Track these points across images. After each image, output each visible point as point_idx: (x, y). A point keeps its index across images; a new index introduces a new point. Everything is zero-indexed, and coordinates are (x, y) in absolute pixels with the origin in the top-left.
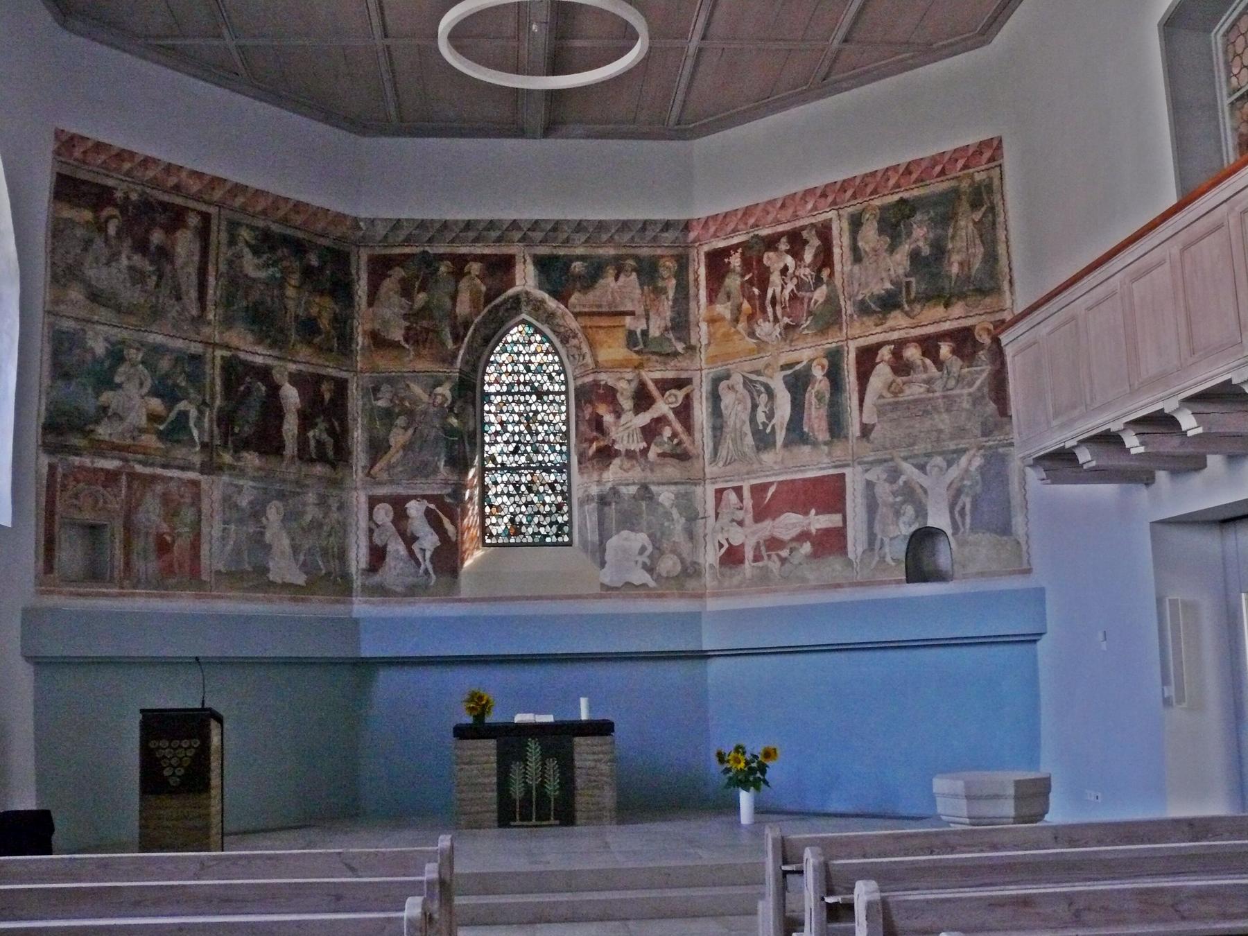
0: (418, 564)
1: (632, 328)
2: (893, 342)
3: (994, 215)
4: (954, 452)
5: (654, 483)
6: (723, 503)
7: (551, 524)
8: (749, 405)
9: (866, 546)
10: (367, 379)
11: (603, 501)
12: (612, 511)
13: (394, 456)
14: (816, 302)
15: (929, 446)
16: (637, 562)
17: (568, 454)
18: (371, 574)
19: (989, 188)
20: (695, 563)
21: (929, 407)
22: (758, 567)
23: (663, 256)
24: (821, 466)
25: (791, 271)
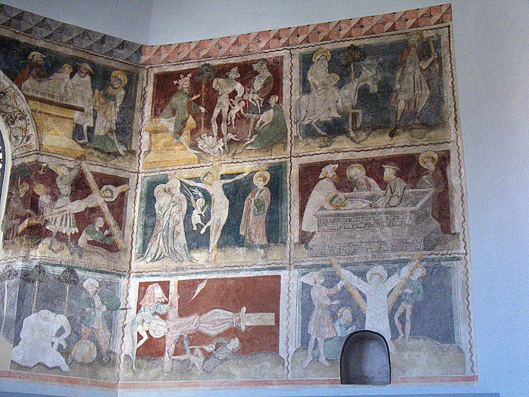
2: (337, 162)
3: (441, 66)
4: (395, 262)
5: (80, 268)
6: (147, 296)
9: (299, 345)
14: (262, 123)
15: (370, 255)
16: (53, 343)
19: (437, 44)
20: (111, 352)
21: (372, 221)
23: (116, 69)
24: (255, 267)
25: (239, 95)
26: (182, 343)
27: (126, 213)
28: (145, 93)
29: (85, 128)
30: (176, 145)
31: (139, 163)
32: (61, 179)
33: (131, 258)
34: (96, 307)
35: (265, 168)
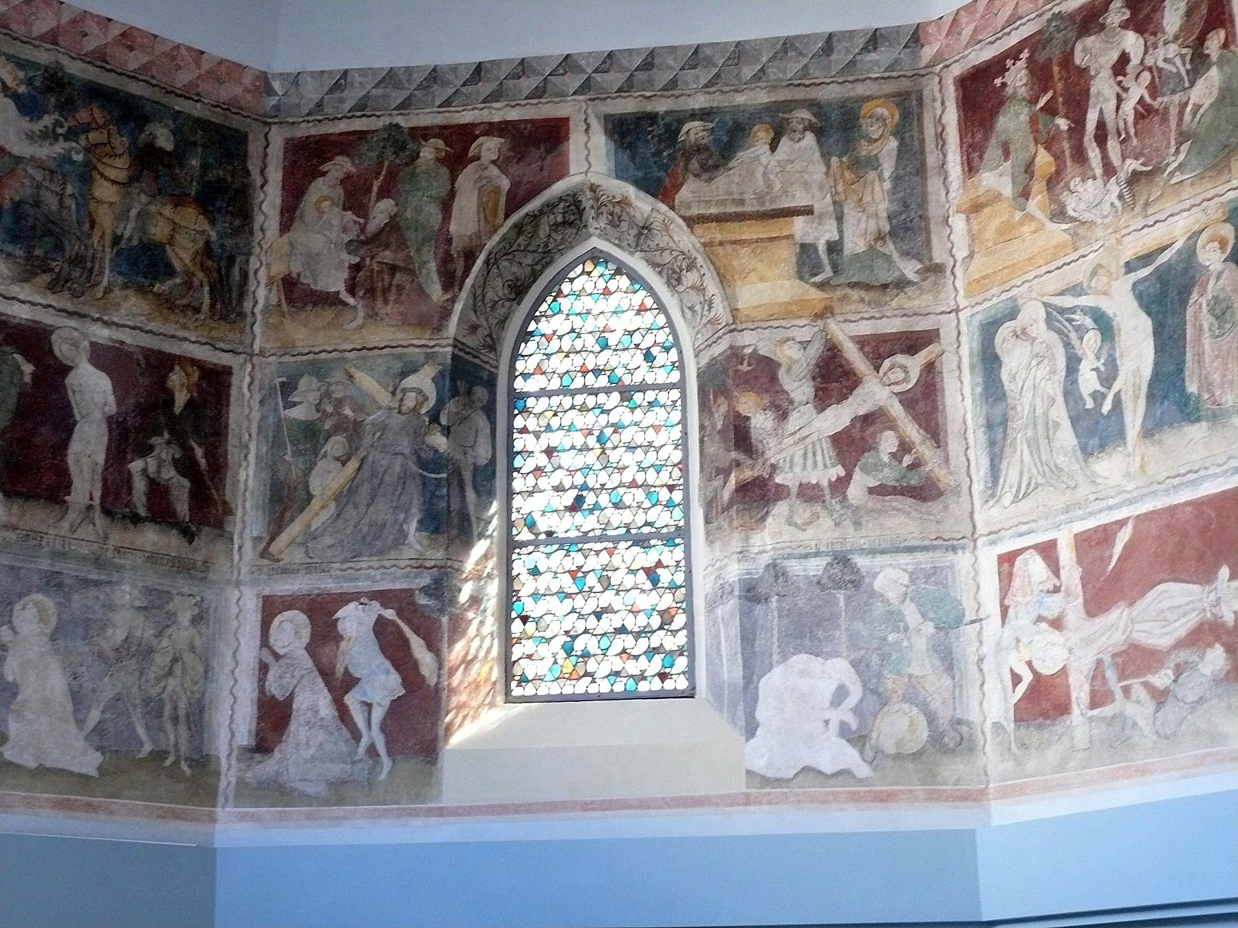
0: (356, 735)
1: (809, 240)
5: (862, 551)
6: (1016, 583)
7: (652, 652)
8: (1062, 362)
10: (273, 368)
11: (751, 593)
12: (770, 615)
13: (318, 514)
14: (1197, 107)
16: (827, 722)
17: (686, 505)
18: (258, 757)
20: (960, 722)
22: (1103, 719)
23: (869, 98)
25: (1135, 60)
26: (1104, 678)
27: (944, 409)
28: (943, 130)
29: (822, 248)
30: (1023, 225)
31: (955, 289)
32: (789, 370)
33: (972, 504)
34: (911, 628)
35: (1220, 215)
